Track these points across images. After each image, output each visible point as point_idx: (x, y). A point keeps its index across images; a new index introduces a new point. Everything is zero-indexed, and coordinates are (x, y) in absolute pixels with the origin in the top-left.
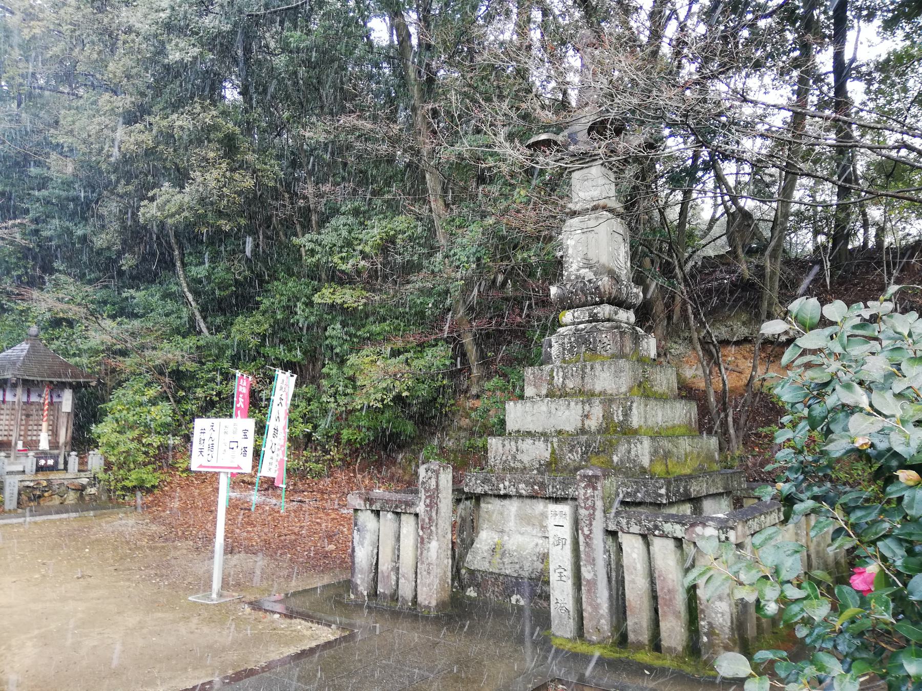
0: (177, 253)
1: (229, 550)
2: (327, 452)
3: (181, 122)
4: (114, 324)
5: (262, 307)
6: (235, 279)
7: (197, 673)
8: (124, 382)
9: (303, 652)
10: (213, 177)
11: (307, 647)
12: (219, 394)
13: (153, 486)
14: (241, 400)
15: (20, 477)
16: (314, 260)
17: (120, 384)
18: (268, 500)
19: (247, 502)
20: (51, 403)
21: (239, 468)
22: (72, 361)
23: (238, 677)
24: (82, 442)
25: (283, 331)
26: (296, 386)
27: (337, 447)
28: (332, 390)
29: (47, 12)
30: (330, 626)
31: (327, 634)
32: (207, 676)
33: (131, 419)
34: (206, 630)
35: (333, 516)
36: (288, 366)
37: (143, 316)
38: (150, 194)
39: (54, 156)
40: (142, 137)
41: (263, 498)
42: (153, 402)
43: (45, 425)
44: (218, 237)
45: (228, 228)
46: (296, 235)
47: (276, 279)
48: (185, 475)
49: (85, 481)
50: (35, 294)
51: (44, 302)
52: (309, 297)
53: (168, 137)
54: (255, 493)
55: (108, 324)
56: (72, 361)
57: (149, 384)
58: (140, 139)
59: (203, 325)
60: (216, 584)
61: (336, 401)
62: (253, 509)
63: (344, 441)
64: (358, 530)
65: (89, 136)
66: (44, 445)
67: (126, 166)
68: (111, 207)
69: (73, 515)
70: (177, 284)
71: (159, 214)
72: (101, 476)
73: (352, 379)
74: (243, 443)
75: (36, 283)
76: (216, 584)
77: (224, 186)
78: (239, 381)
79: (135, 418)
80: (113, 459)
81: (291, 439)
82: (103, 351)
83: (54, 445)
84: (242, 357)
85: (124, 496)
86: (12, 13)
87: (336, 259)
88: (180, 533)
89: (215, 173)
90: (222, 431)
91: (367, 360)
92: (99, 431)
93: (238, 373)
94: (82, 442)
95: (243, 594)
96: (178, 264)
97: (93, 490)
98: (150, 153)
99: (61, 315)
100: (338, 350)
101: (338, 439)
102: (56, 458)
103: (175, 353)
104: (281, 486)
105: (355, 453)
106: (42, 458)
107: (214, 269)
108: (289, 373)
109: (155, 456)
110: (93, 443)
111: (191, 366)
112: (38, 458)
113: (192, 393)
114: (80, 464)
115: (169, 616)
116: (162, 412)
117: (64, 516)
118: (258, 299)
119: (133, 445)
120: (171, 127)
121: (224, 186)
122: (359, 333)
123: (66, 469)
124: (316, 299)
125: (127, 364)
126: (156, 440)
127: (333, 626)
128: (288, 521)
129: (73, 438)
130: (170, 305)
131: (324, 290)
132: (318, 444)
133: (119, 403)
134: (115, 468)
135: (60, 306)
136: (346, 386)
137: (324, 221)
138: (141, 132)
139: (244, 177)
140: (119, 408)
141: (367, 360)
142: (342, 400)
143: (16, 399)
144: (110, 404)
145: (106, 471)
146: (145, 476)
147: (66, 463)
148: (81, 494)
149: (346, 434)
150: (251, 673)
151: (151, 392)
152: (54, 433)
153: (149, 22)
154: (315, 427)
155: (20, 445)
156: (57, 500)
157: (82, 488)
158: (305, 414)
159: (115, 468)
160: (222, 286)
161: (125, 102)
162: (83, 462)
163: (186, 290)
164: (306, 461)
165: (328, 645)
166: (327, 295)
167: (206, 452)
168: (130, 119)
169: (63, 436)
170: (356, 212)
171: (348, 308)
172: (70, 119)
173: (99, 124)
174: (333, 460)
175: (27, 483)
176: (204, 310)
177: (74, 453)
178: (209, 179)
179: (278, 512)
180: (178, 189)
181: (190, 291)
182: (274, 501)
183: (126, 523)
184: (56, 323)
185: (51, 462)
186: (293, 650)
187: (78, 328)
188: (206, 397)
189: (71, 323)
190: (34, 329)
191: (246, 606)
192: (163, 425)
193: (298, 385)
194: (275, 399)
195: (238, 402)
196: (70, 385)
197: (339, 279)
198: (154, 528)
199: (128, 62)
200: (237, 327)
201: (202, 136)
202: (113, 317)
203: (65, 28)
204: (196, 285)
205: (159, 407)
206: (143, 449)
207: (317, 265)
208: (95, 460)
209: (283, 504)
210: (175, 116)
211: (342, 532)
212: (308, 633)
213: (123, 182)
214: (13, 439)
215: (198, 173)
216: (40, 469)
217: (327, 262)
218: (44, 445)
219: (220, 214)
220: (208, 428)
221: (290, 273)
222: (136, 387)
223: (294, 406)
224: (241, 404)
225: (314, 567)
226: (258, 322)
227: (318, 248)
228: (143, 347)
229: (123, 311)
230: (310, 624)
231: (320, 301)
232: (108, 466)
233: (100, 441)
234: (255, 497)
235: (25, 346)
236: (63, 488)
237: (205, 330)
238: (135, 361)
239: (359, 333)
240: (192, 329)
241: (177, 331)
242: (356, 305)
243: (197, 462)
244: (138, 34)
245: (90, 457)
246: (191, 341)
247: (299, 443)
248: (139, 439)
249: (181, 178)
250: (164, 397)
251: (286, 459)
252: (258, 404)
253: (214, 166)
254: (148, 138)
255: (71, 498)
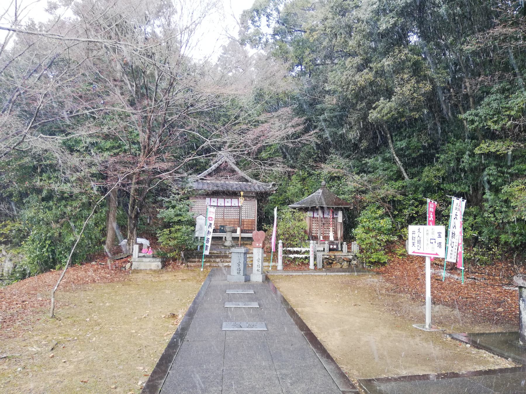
0: (389, 136)
1: (434, 303)
2: (490, 249)
3: (387, 62)
4: (359, 177)
5: (440, 160)
6: (423, 146)
7: (424, 368)
8: (366, 206)
9: (490, 370)
10: (407, 89)
11: (493, 368)
12: (417, 213)
13: (385, 263)
14: (431, 216)
15: (322, 253)
16: (474, 126)
17: (364, 208)
18: (453, 276)
19: (439, 276)
20: (333, 218)
21: (437, 254)
22: (342, 197)
23: (446, 376)
24: (348, 237)
25: (453, 175)
26: (465, 208)
27: (497, 246)
28: (491, 210)
29: (319, 26)
30: (507, 359)
31: (507, 364)
32: (430, 371)
33: (371, 226)
34: (425, 344)
35: (499, 290)
36: (458, 195)
37: (373, 172)
38: (374, 106)
39: (327, 96)
40: (367, 77)
41: (449, 274)
42: (382, 217)
43: (331, 228)
44: (412, 122)
45: (417, 116)
46: (461, 114)
47: (449, 142)
48: (401, 257)
49: (351, 257)
50: (323, 165)
51: (327, 169)
52: (472, 151)
53: (380, 73)
54: (444, 271)
55: (357, 177)
56: (342, 197)
57: (378, 208)
58: (367, 77)
59: (405, 174)
60: (428, 320)
61: (495, 216)
62: (443, 280)
63: (502, 242)
64: (523, 300)
65: (342, 82)
66: (332, 238)
67: (359, 95)
68: (353, 117)
69: (347, 273)
70: (389, 153)
71: (379, 115)
72: (358, 255)
73: (507, 201)
74: (438, 240)
75: (324, 160)
76: (428, 320)
77: (414, 92)
78: (429, 205)
79: (373, 226)
80: (364, 247)
81: (465, 240)
82: (355, 192)
83: (336, 238)
84: (429, 190)
85: (370, 266)
86: (305, 32)
87: (489, 123)
88: (402, 289)
89: (409, 86)
90: (425, 233)
91: (516, 189)
92: (356, 232)
93: (428, 200)
94: (348, 237)
95: (444, 329)
96: (390, 141)
97: (355, 262)
98: (371, 83)
99: (335, 175)
100: (493, 183)
101: (497, 241)
102: (337, 245)
103: (389, 190)
104: (461, 268)
105: (512, 251)
106: (331, 244)
107: (410, 141)
108: (461, 199)
109: (384, 246)
110: (353, 238)
111: (400, 197)
112: (330, 245)
113: (404, 212)
114: (348, 248)
115: (404, 333)
116: (386, 223)
117: (343, 274)
118: (437, 155)
119: (373, 240)
120: (383, 66)
121: (414, 92)
122: (510, 171)
123: (342, 250)
124: (477, 151)
125: (367, 197)
126: (384, 238)
127: (509, 359)
128: (467, 290)
129: (344, 235)
130: (387, 165)
131: (482, 145)
132: (483, 244)
133: (364, 218)
134: (365, 251)
135: (334, 170)
136: (502, 207)
137: (478, 101)
138: (367, 73)
139: (425, 84)
140: (365, 220)
141: (516, 189)
142: (499, 216)
143: (318, 216)
144: (360, 218)
145: (360, 253)
146: (380, 257)
147: (342, 247)
148: (350, 264)
149: (503, 237)
150: (455, 375)
151: (380, 212)
152: (335, 233)
153: (368, 12)
154: (480, 233)
155: (321, 239)
156: (339, 266)
157: (349, 261)
158: (472, 225)
159: (365, 251)
160: (417, 149)
161: (358, 60)
162: (349, 248)
163: (395, 155)
164: (475, 254)
165: (506, 370)
166: (486, 147)
167: (416, 244)
168: (359, 69)
169: (340, 234)
170: (503, 91)
171: (500, 154)
172: (333, 76)
173: (347, 75)
174: (494, 254)
175: (326, 256)
176: (405, 165)
177: (345, 243)
178: (405, 89)
179: (460, 284)
180: (388, 100)
181: (397, 156)
182: (456, 277)
183: (372, 280)
184: (333, 178)
185: (335, 247)
186: (482, 368)
187: (343, 181)
188: (410, 214)
189: (339, 178)
190: (323, 183)
191: (448, 336)
192: (389, 230)
193: (467, 206)
194: (453, 215)
195: (430, 217)
196: (341, 209)
197: (492, 136)
198: (388, 284)
199: (358, 37)
200: (426, 173)
201: (399, 69)
202: (358, 174)
203: (328, 30)
204: (400, 153)
205: (384, 220)
206: (378, 242)
207: (475, 130)
208: (355, 247)
209: (463, 279)
210: (384, 60)
211: (507, 301)
212: (492, 360)
213: (359, 103)
214: (318, 235)
215: (399, 89)
216: (330, 250)
217: (484, 126)
218: (332, 238)
219: (411, 110)
220: (417, 231)
221: (458, 137)
222: (372, 210)
223: (465, 220)
224: (431, 218)
225: (489, 320)
226: (438, 170)
227: (476, 118)
228: (374, 189)
229: (362, 170)
230: (492, 355)
231: (479, 152)
232: (361, 251)
233: (357, 237)
234: (444, 274)
235: (320, 191)
236: (341, 260)
237: (406, 176)
238: (371, 195)
239: (510, 171)
240: (399, 176)
241: (390, 179)
242: (506, 152)
243: (412, 249)
244: (363, 21)
245: (352, 245)
246: (399, 183)
247: (469, 243)
248: (375, 237)
249: (389, 94)
250: (386, 214)
251: (463, 252)
252: (442, 218)
253: (407, 82)
254: (371, 76)
255: (345, 265)
